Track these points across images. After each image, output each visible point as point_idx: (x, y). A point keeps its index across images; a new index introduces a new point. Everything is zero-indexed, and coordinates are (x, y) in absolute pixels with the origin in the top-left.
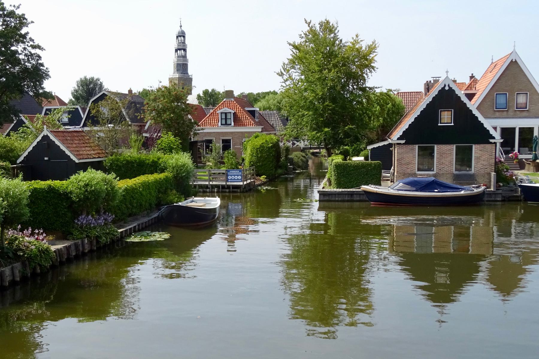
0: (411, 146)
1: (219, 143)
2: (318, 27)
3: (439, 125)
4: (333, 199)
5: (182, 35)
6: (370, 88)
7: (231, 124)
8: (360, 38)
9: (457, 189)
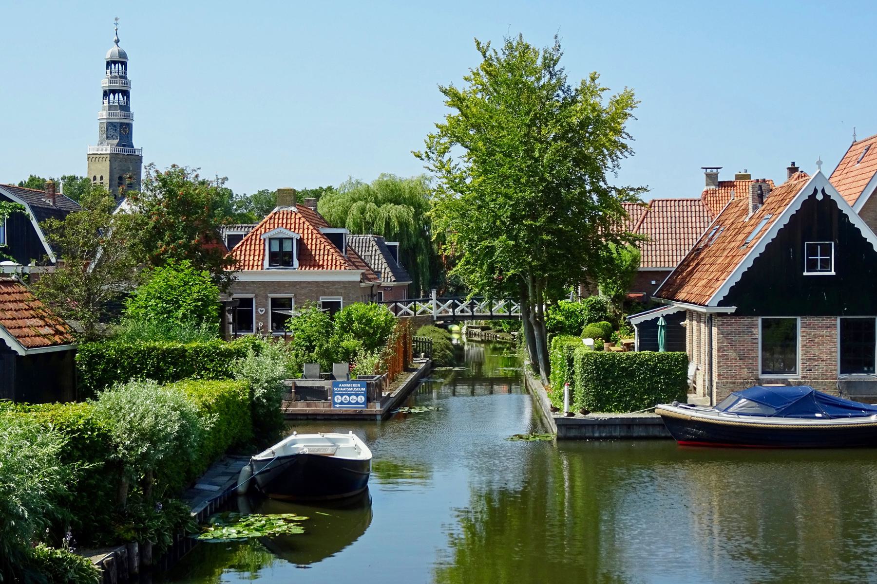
0: (747, 320)
1: (265, 306)
3: (805, 274)
5: (119, 61)
6: (620, 192)
8: (600, 83)
9: (857, 412)
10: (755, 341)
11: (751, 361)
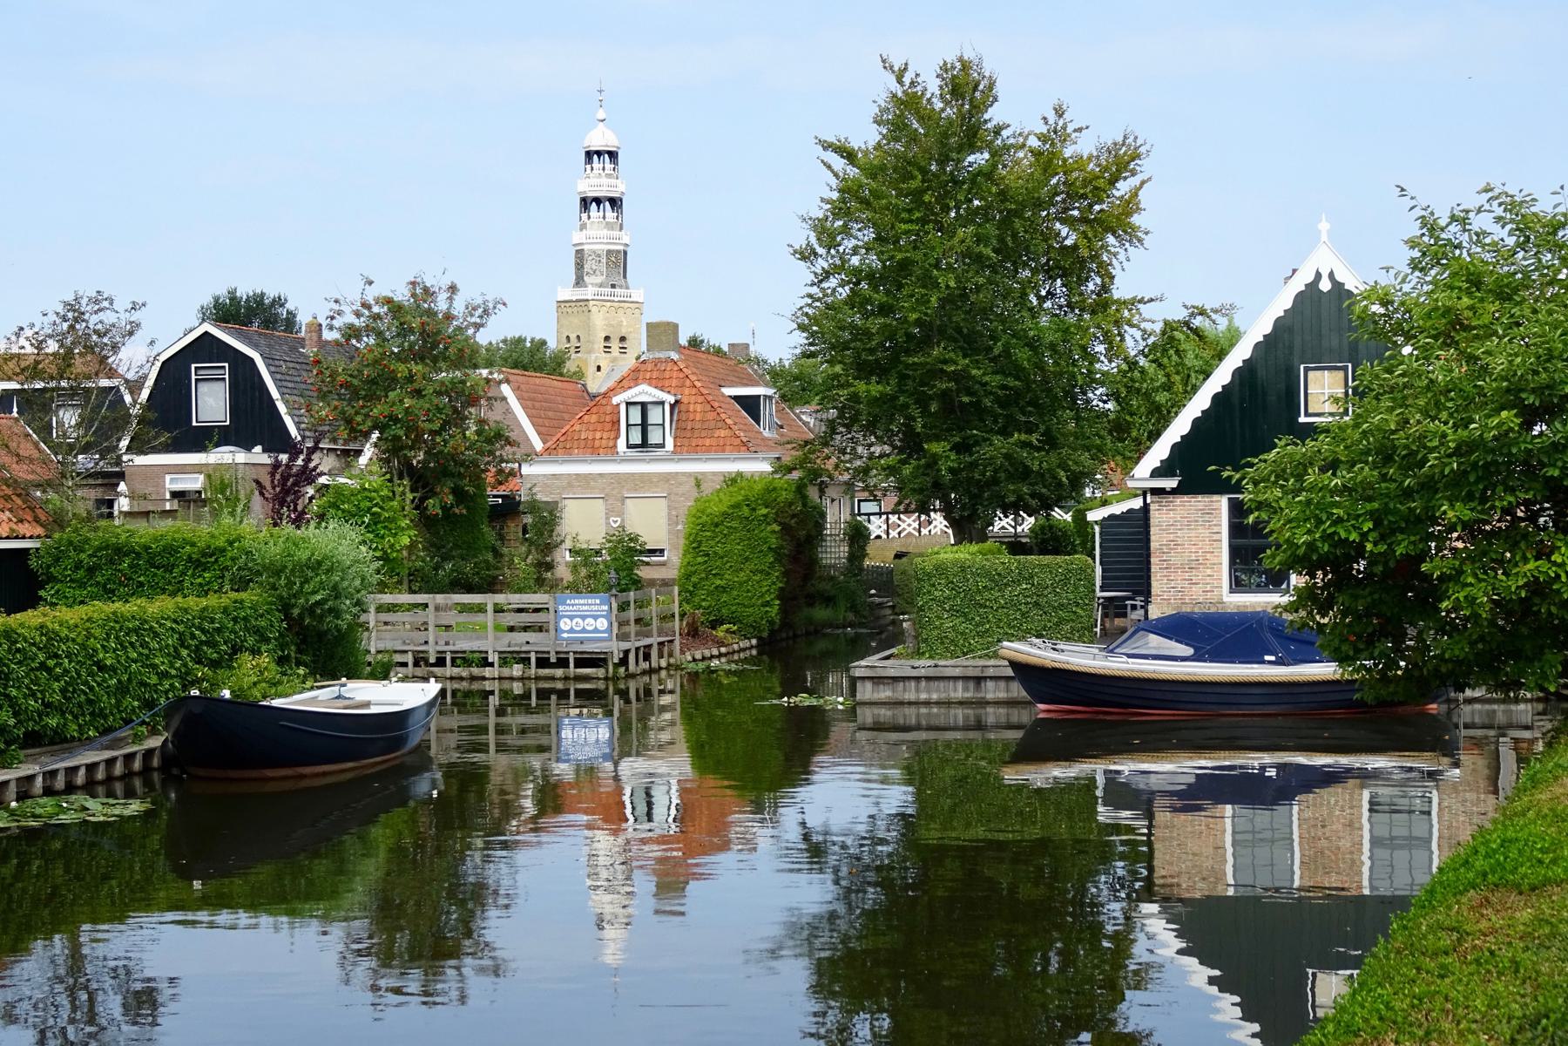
0: (1201, 501)
2: (932, 86)
3: (1302, 419)
4: (911, 696)
7: (662, 446)
8: (1074, 118)
10: (1216, 537)
11: (1209, 572)
